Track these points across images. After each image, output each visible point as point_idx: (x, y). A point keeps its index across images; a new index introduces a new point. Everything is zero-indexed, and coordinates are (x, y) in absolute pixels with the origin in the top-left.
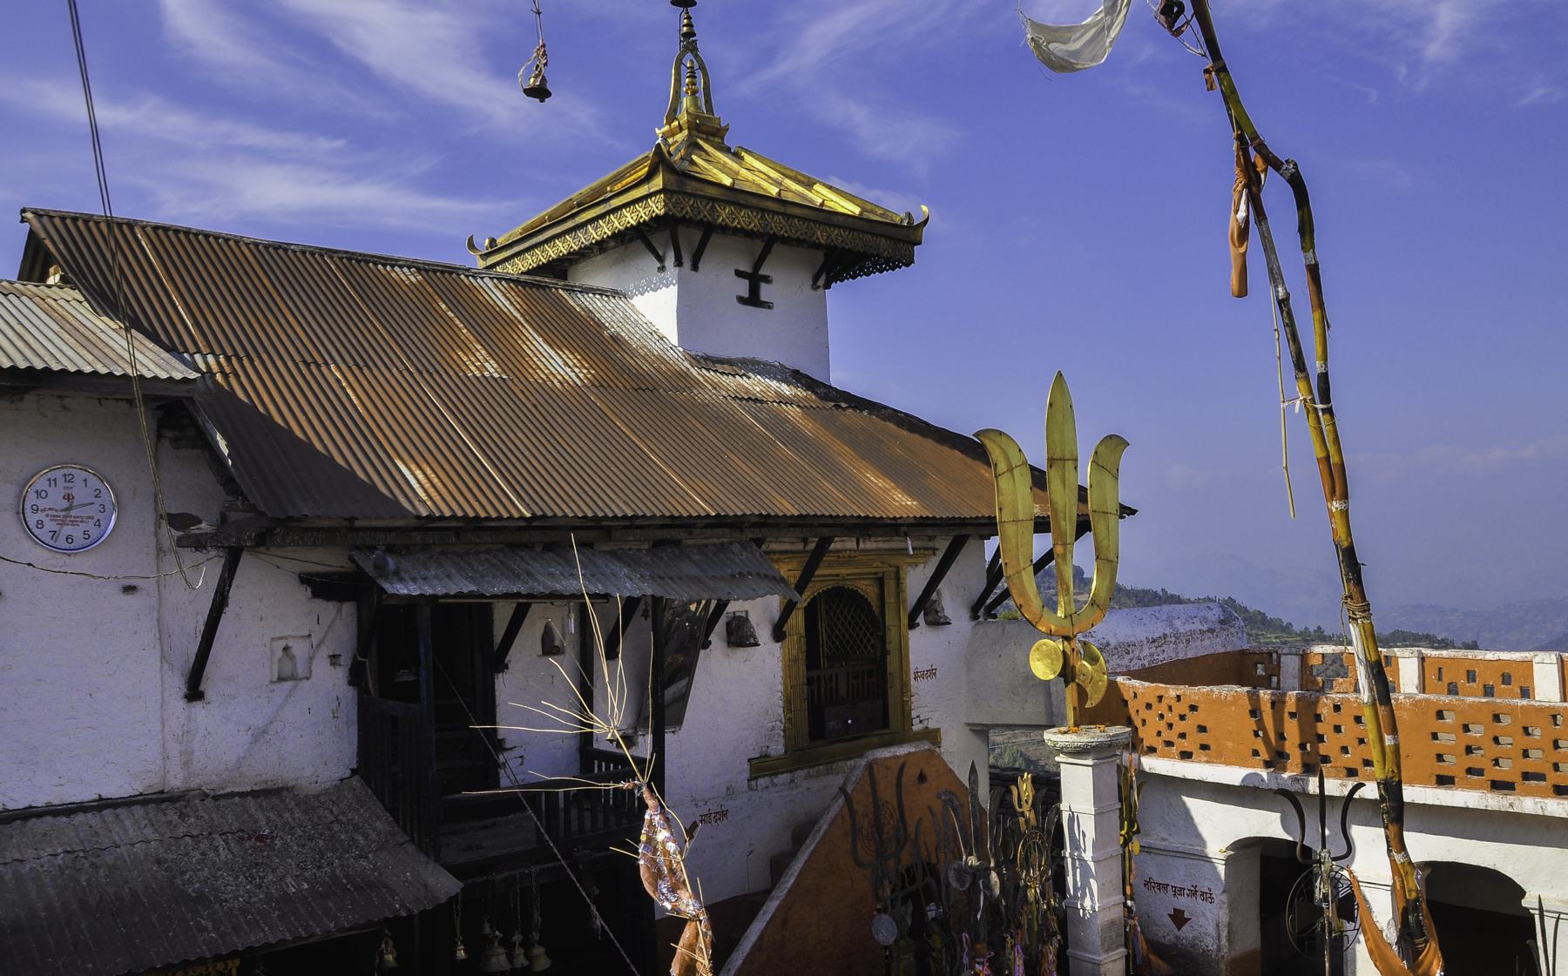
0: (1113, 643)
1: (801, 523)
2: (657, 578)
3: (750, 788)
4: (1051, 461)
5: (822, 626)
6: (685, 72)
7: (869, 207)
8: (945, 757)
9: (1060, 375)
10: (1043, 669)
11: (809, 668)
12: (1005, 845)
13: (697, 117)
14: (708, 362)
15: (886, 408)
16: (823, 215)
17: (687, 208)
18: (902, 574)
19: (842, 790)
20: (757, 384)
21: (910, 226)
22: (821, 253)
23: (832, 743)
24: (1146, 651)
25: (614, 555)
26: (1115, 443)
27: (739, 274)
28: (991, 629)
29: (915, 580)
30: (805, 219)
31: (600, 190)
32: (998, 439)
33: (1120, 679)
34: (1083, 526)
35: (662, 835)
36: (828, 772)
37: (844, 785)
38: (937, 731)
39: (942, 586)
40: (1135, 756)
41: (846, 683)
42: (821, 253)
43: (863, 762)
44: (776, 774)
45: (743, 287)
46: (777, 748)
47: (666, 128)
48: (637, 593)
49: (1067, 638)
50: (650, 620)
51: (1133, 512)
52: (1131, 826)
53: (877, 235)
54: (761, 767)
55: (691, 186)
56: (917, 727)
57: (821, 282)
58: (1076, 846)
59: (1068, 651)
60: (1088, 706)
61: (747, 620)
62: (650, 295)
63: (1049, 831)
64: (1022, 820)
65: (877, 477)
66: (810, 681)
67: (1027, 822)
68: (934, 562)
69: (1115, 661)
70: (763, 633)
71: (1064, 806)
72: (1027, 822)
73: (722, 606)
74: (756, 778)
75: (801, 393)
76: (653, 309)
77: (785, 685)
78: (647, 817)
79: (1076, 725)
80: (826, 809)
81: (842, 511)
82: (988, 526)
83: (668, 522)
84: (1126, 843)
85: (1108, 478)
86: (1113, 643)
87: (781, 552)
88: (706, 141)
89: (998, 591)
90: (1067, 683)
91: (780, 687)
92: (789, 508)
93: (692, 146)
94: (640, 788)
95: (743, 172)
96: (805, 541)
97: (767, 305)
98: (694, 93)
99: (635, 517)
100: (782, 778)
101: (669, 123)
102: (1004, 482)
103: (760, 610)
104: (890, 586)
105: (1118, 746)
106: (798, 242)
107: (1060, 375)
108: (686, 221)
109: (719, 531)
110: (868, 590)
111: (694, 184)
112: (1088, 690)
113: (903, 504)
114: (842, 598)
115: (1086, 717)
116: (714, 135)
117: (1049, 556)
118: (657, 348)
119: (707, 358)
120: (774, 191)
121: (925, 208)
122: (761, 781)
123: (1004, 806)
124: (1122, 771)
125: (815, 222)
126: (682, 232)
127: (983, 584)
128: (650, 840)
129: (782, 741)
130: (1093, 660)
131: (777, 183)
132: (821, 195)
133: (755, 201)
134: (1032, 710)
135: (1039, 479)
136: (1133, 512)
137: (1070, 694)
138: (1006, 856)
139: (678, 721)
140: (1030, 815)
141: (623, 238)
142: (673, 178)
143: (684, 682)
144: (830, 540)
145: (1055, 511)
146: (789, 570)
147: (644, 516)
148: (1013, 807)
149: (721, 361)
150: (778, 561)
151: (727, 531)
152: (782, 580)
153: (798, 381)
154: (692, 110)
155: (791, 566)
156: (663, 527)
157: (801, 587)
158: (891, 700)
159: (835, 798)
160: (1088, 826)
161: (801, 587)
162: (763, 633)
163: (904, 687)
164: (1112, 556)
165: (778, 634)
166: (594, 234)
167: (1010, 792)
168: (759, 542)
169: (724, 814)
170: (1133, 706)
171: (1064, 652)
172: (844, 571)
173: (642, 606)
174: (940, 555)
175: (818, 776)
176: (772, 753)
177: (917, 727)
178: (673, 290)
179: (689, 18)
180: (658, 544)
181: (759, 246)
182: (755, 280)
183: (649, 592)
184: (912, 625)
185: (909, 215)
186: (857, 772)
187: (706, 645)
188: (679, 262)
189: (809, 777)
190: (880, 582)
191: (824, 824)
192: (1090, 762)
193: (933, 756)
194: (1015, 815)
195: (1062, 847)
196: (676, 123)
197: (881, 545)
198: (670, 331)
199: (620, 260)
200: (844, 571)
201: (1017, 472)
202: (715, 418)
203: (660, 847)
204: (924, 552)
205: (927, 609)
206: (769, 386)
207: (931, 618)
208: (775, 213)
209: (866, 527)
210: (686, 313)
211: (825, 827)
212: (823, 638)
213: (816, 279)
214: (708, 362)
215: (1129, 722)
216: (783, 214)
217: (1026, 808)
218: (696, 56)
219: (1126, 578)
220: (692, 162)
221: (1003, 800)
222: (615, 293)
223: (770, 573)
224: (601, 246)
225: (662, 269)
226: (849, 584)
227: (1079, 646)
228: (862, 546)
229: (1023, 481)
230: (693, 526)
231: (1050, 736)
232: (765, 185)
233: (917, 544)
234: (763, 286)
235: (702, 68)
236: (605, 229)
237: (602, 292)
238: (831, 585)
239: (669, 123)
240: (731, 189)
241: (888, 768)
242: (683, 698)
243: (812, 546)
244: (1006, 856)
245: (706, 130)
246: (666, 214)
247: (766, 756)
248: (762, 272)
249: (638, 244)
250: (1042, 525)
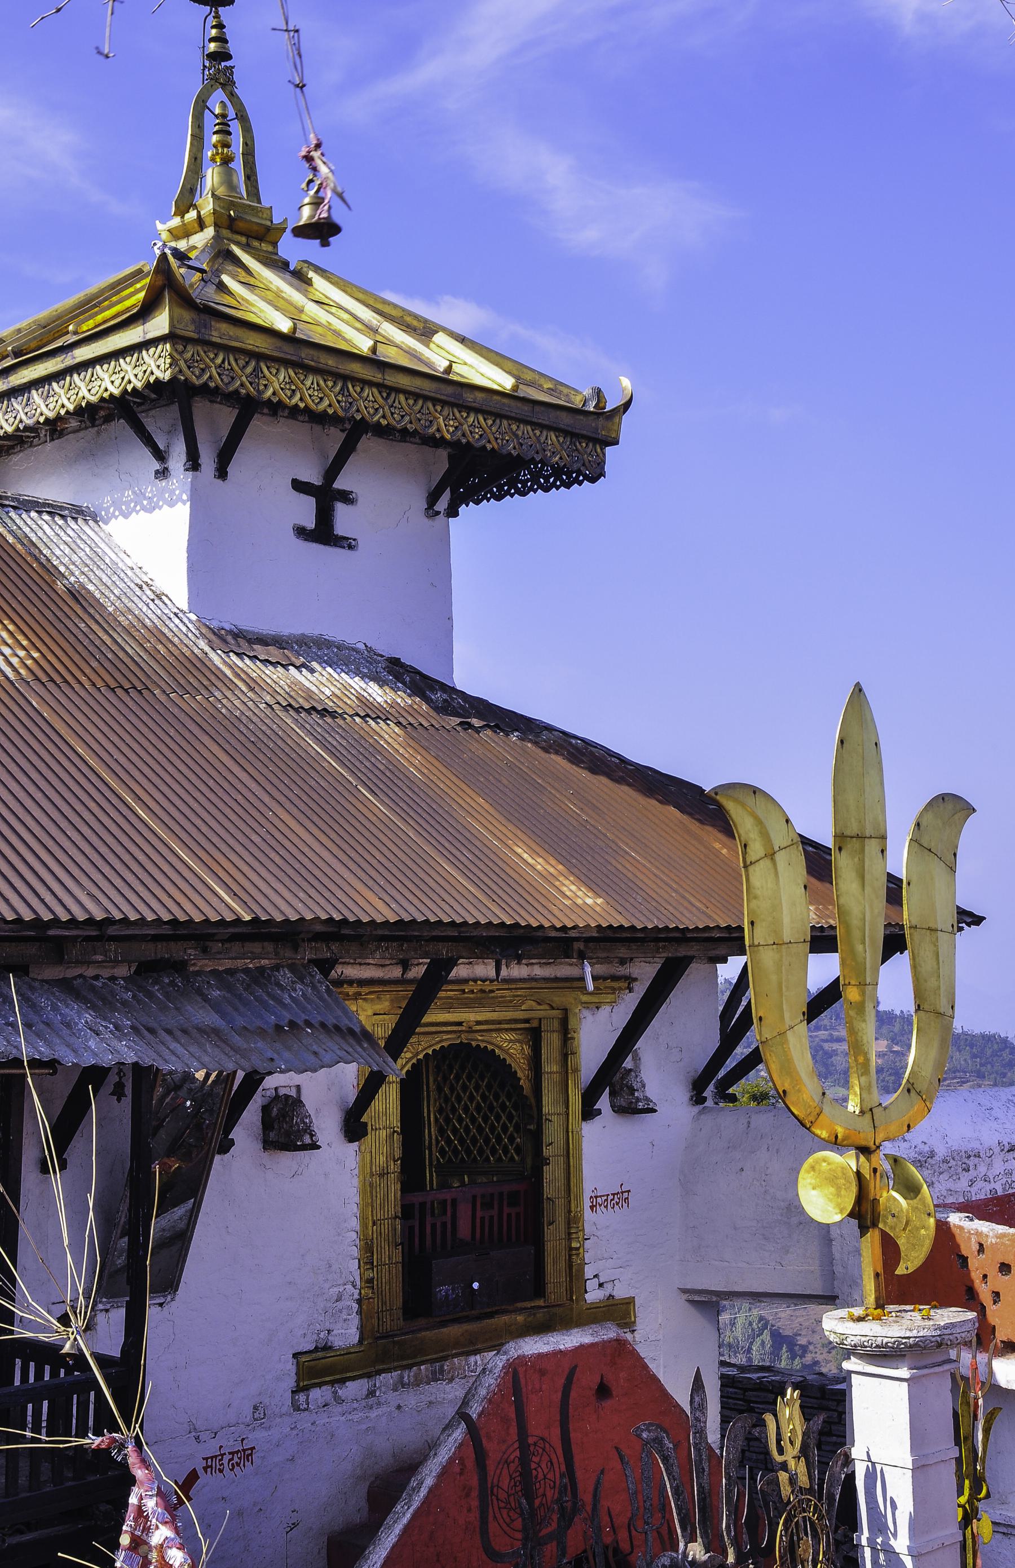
0: (941, 1152)
1: (401, 936)
2: (142, 1031)
3: (297, 1408)
4: (840, 837)
5: (430, 1112)
6: (210, 123)
7: (529, 376)
8: (643, 1351)
9: (858, 689)
10: (822, 1203)
11: (407, 1187)
12: (753, 1526)
13: (232, 205)
14: (239, 640)
15: (549, 728)
16: (450, 390)
17: (212, 370)
18: (572, 1023)
19: (462, 1415)
20: (324, 683)
21: (600, 413)
22: (443, 454)
23: (443, 1324)
24: (998, 1167)
25: (68, 988)
26: (950, 809)
27: (299, 486)
28: (727, 1120)
29: (595, 1034)
30: (417, 396)
31: (54, 327)
32: (750, 800)
33: (955, 1219)
34: (894, 943)
35: (161, 1534)
36: (435, 1377)
37: (465, 1402)
38: (630, 1302)
39: (643, 1044)
40: (982, 1358)
41: (474, 1221)
42: (443, 454)
43: (497, 1362)
44: (343, 1381)
45: (304, 511)
46: (347, 1334)
47: (176, 221)
48: (108, 1060)
49: (864, 1151)
50: (127, 1101)
51: (977, 920)
52: (976, 1488)
53: (542, 427)
54: (318, 1368)
55: (220, 332)
56: (593, 1295)
57: (442, 505)
58: (879, 1526)
59: (866, 1173)
60: (900, 1271)
61: (298, 1102)
62: (140, 519)
63: (831, 1497)
64: (783, 1476)
65: (534, 853)
66: (407, 1212)
67: (793, 1480)
68: (629, 1003)
69: (944, 1184)
70: (327, 1126)
71: (857, 1452)
72: (793, 1480)
73: (253, 1081)
74: (306, 1389)
75: (402, 699)
76: (142, 543)
77: (363, 1219)
78: (133, 1500)
79: (880, 1305)
80: (432, 1447)
81: (472, 915)
82: (730, 940)
83: (166, 930)
84: (968, 1518)
85: (938, 869)
86: (941, 1152)
87: (362, 983)
88: (247, 248)
89: (741, 1051)
90: (863, 1229)
91: (355, 1223)
92: (378, 907)
93: (222, 255)
94: (122, 1446)
95: (312, 310)
96: (405, 965)
97: (346, 543)
98: (226, 161)
99: (109, 921)
100: (355, 1388)
101: (181, 212)
102: (760, 876)
103: (324, 1088)
104: (551, 1043)
105: (952, 1345)
106: (405, 435)
107: (858, 689)
108: (209, 392)
109: (256, 947)
110: (511, 1048)
111: (224, 327)
112: (901, 1242)
113: (578, 902)
114: (466, 1062)
115: (898, 1291)
116: (260, 239)
117: (831, 994)
118: (150, 613)
119: (238, 635)
120: (363, 344)
121: (626, 382)
122: (316, 1394)
123: (755, 1455)
124: (961, 1386)
125: (435, 401)
126: (200, 408)
127: (713, 1042)
128: (138, 1543)
129: (355, 1320)
130: (911, 1190)
131: (371, 330)
132: (442, 354)
133: (331, 362)
134: (800, 1271)
135: (818, 861)
136: (977, 920)
137: (870, 1247)
138: (755, 1540)
139: (169, 1284)
140: (800, 1469)
141: (91, 415)
142: (187, 315)
143: (180, 1211)
144: (452, 963)
145: (842, 913)
146: (374, 1015)
147: (125, 921)
148: (767, 1453)
149: (263, 641)
150: (357, 996)
151: (270, 947)
152: (366, 1036)
153: (398, 678)
154: (221, 191)
155: (378, 1007)
156: (156, 938)
157: (395, 1045)
158: (549, 1246)
159: (448, 1427)
160: (900, 1488)
161: (395, 1045)
162: (327, 1126)
163: (573, 1222)
164: (943, 1006)
165: (354, 1127)
166: (42, 406)
167: (763, 1424)
168: (325, 966)
169: (248, 1454)
170: (977, 1266)
171: (858, 1174)
172: (470, 1016)
173: (113, 1078)
174: (640, 989)
175: (417, 1383)
176: (338, 1342)
177: (593, 1295)
178: (182, 512)
179: (220, 26)
180: (147, 970)
181: (335, 438)
182: (326, 497)
183: (130, 1058)
184: (589, 1113)
185: (598, 393)
186: (490, 1381)
187: (226, 1146)
188: (193, 463)
189: (401, 1385)
190: (534, 1035)
191: (428, 1476)
192: (904, 1373)
193: (621, 1352)
194: (769, 1466)
195: (854, 1525)
196: (192, 215)
197: (538, 971)
198: (176, 587)
199: (88, 455)
200: (470, 1016)
201: (781, 858)
202: (251, 743)
203: (154, 1556)
204: (614, 983)
205: (615, 1084)
206: (346, 687)
207: (622, 1102)
208: (365, 383)
209: (511, 941)
210: (207, 552)
211: (429, 1482)
212: (431, 1132)
213: (433, 498)
214: (239, 640)
215: (969, 1298)
216: (380, 386)
217: (791, 1452)
218: (232, 95)
219: (967, 1019)
220: (222, 287)
221: (750, 1439)
222: (78, 512)
223: (344, 1023)
224: (55, 427)
225: (163, 473)
226: (479, 1040)
227: (887, 1166)
228: (504, 972)
229: (792, 868)
230: (211, 937)
231: (836, 1324)
232: (350, 333)
233: (601, 969)
234: (341, 509)
235: (242, 117)
236: (63, 399)
237: (53, 510)
238: (447, 1040)
239: (181, 212)
240: (289, 339)
241: (542, 1373)
242: (180, 1241)
243: (417, 972)
244: (755, 1540)
245: (245, 228)
246: (173, 380)
247: (327, 1348)
248: (339, 484)
249: (120, 427)
250: (823, 941)
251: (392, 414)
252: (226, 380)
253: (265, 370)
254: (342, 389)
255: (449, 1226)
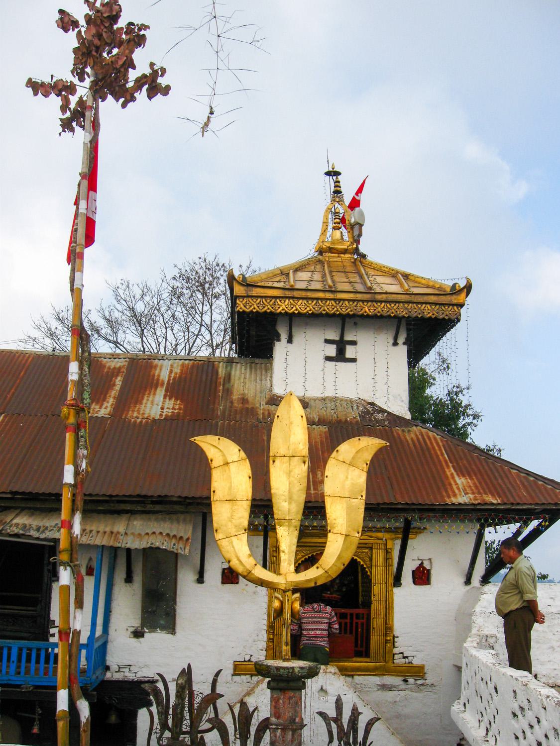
125: (363, 301)
177: (399, 660)
216: (334, 300)
251: (341, 309)
252: (290, 308)
253: (279, 302)
254: (316, 303)
255: (348, 625)
